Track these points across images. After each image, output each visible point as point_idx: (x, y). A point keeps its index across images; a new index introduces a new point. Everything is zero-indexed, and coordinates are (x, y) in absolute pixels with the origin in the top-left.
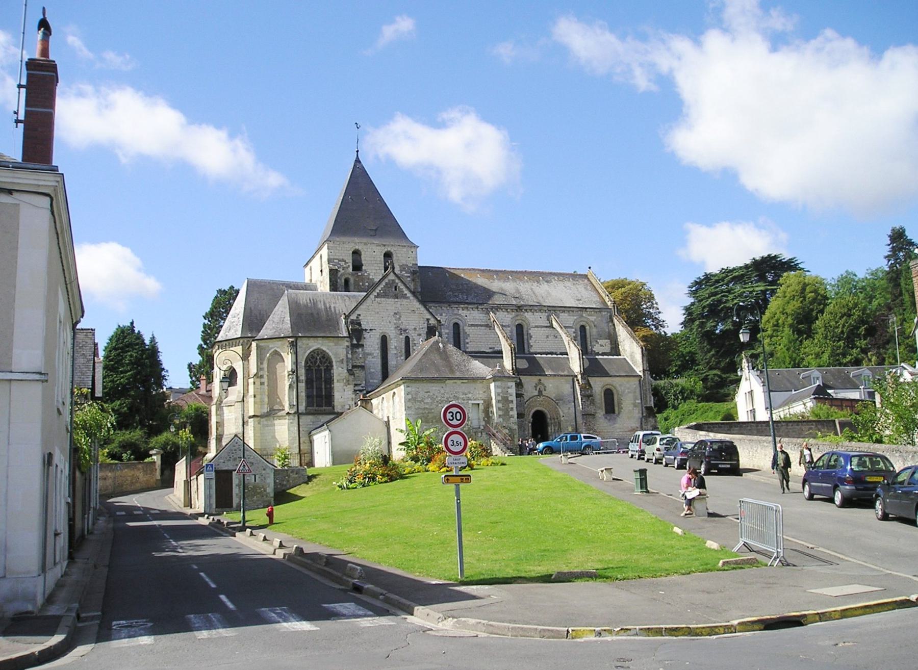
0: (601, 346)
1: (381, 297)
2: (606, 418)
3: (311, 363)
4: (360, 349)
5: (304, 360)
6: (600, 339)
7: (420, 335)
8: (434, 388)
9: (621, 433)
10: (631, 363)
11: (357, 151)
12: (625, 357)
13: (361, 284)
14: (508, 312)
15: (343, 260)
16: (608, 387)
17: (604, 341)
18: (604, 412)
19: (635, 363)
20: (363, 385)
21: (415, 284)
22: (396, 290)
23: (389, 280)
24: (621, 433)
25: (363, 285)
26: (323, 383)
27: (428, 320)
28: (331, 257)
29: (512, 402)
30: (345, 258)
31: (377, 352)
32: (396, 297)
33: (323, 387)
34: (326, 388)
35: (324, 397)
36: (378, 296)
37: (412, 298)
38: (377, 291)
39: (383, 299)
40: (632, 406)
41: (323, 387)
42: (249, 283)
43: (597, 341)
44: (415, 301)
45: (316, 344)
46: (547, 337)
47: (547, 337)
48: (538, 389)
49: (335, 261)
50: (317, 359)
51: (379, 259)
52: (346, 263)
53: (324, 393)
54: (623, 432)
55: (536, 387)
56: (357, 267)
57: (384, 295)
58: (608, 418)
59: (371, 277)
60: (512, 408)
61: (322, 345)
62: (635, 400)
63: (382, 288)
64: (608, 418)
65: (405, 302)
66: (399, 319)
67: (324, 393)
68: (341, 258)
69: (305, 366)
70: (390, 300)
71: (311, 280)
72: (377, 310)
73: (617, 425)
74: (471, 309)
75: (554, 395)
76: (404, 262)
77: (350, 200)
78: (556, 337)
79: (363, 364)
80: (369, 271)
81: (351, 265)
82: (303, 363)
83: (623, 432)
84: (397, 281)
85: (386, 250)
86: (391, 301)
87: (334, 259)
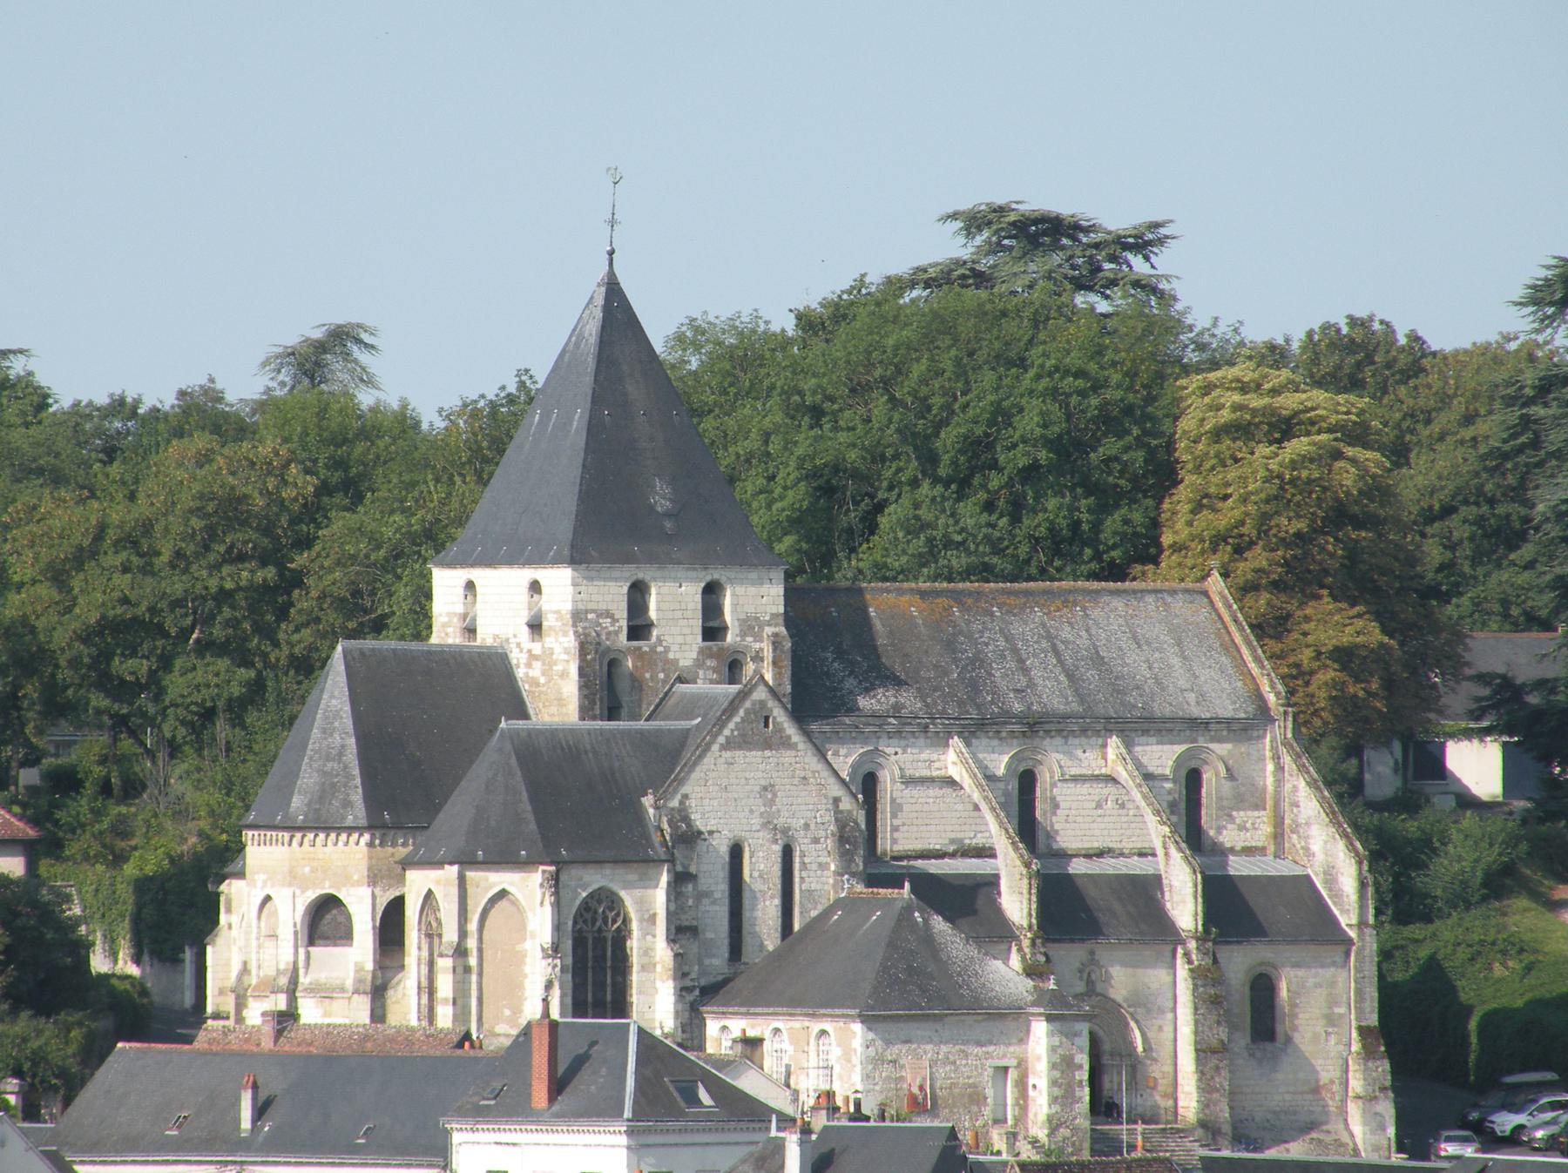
0: (1242, 828)
1: (735, 749)
2: (1252, 1055)
3: (585, 922)
4: (690, 887)
5: (571, 917)
6: (1238, 810)
7: (816, 841)
8: (919, 1032)
9: (1288, 1097)
10: (1324, 893)
11: (611, 253)
12: (1310, 872)
13: (647, 675)
14: (1001, 739)
15: (608, 614)
16: (1262, 969)
17: (1249, 813)
18: (1248, 1039)
19: (1337, 895)
20: (693, 975)
21: (780, 673)
22: (766, 725)
23: (753, 704)
24: (1288, 1097)
25: (652, 678)
26: (609, 973)
27: (836, 801)
28: (581, 606)
29: (1081, 1067)
30: (613, 607)
31: (721, 889)
32: (767, 745)
33: (609, 981)
34: (614, 984)
35: (609, 1006)
36: (727, 746)
37: (801, 746)
38: (727, 732)
39: (738, 753)
40: (1323, 1022)
41: (609, 981)
42: (349, 657)
43: (1230, 816)
44: (809, 753)
45: (599, 877)
46: (1099, 806)
47: (1099, 806)
48: (1085, 976)
49: (590, 616)
50: (596, 912)
51: (691, 606)
52: (614, 620)
53: (609, 997)
54: (1294, 1093)
55: (1081, 971)
56: (639, 629)
57: (741, 742)
58: (1258, 1054)
59: (671, 656)
60: (1081, 1081)
61: (612, 881)
62: (1330, 1008)
63: (737, 723)
64: (1258, 1054)
65: (787, 756)
66: (772, 802)
67: (609, 997)
68: (603, 606)
69: (573, 931)
70: (754, 753)
71: (471, 631)
72: (725, 782)
73: (1280, 1076)
74: (909, 735)
75: (1124, 992)
76: (750, 609)
77: (607, 419)
78: (1122, 806)
79: (695, 923)
80: (668, 640)
81: (624, 623)
82: (570, 923)
83: (1294, 1093)
84: (771, 704)
85: (709, 578)
86: (755, 756)
87: (587, 612)
